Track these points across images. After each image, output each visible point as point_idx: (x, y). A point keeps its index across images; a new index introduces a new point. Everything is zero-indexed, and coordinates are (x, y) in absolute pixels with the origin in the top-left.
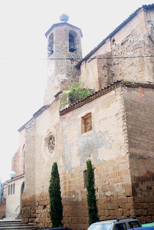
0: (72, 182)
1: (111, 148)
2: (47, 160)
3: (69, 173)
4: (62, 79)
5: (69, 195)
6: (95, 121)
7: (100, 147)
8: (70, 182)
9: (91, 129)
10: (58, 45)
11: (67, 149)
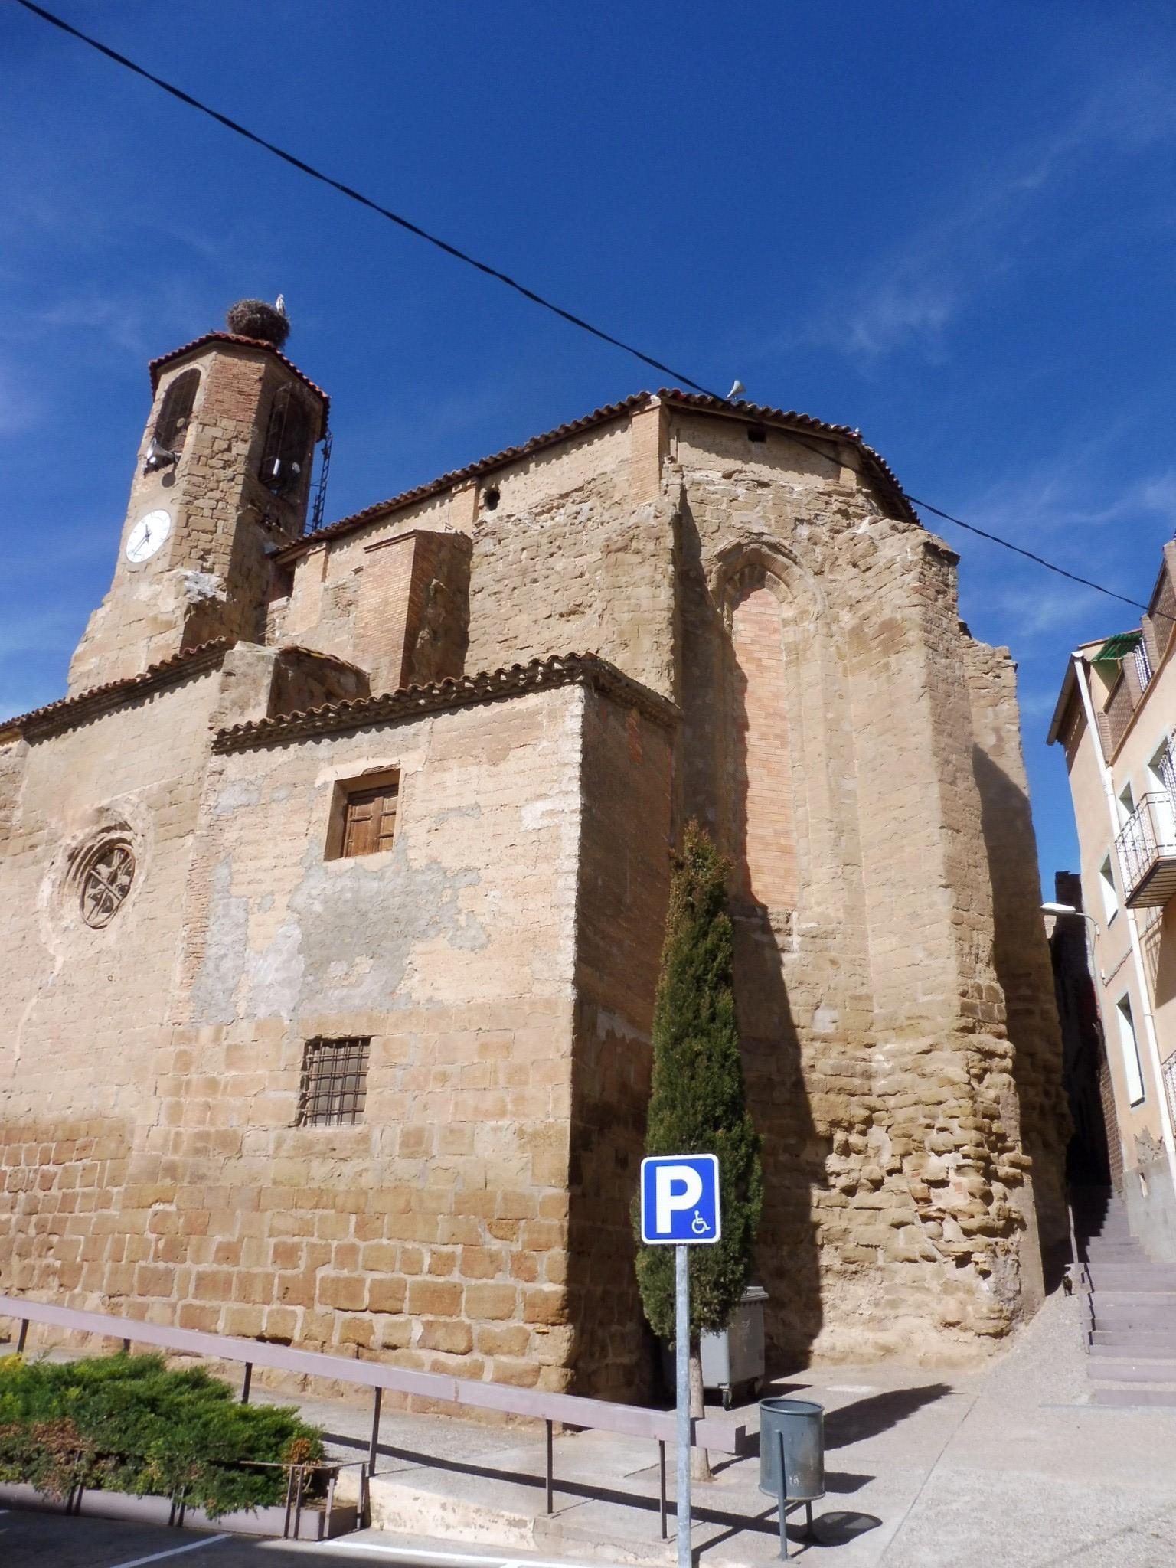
0: (226, 1087)
1: (483, 947)
2: (60, 961)
3: (216, 1039)
4: (200, 593)
5: (198, 1151)
6: (411, 805)
7: (422, 936)
8: (212, 1085)
9: (378, 841)
10: (211, 432)
11: (223, 921)
